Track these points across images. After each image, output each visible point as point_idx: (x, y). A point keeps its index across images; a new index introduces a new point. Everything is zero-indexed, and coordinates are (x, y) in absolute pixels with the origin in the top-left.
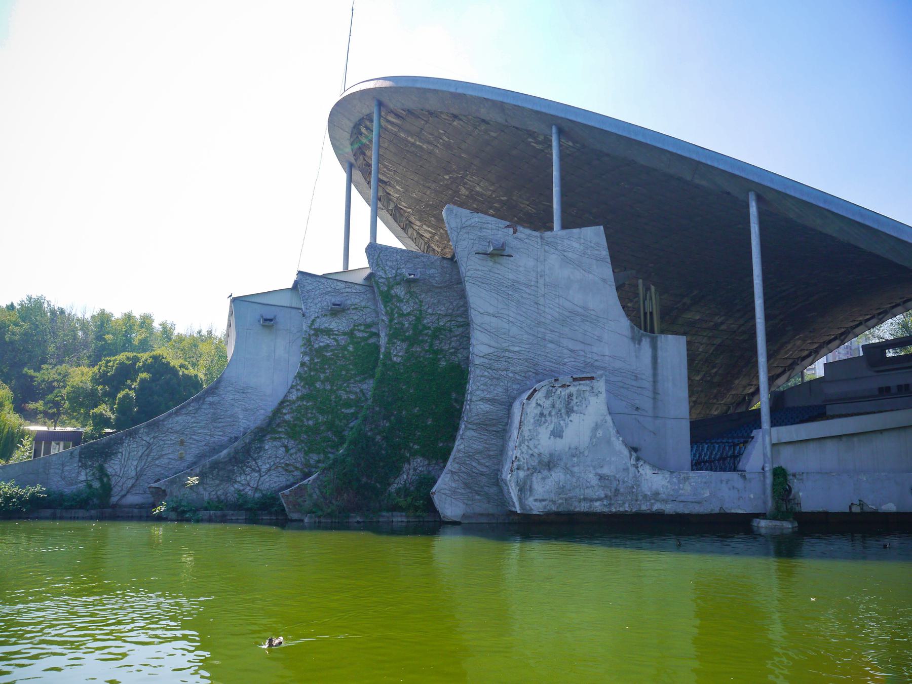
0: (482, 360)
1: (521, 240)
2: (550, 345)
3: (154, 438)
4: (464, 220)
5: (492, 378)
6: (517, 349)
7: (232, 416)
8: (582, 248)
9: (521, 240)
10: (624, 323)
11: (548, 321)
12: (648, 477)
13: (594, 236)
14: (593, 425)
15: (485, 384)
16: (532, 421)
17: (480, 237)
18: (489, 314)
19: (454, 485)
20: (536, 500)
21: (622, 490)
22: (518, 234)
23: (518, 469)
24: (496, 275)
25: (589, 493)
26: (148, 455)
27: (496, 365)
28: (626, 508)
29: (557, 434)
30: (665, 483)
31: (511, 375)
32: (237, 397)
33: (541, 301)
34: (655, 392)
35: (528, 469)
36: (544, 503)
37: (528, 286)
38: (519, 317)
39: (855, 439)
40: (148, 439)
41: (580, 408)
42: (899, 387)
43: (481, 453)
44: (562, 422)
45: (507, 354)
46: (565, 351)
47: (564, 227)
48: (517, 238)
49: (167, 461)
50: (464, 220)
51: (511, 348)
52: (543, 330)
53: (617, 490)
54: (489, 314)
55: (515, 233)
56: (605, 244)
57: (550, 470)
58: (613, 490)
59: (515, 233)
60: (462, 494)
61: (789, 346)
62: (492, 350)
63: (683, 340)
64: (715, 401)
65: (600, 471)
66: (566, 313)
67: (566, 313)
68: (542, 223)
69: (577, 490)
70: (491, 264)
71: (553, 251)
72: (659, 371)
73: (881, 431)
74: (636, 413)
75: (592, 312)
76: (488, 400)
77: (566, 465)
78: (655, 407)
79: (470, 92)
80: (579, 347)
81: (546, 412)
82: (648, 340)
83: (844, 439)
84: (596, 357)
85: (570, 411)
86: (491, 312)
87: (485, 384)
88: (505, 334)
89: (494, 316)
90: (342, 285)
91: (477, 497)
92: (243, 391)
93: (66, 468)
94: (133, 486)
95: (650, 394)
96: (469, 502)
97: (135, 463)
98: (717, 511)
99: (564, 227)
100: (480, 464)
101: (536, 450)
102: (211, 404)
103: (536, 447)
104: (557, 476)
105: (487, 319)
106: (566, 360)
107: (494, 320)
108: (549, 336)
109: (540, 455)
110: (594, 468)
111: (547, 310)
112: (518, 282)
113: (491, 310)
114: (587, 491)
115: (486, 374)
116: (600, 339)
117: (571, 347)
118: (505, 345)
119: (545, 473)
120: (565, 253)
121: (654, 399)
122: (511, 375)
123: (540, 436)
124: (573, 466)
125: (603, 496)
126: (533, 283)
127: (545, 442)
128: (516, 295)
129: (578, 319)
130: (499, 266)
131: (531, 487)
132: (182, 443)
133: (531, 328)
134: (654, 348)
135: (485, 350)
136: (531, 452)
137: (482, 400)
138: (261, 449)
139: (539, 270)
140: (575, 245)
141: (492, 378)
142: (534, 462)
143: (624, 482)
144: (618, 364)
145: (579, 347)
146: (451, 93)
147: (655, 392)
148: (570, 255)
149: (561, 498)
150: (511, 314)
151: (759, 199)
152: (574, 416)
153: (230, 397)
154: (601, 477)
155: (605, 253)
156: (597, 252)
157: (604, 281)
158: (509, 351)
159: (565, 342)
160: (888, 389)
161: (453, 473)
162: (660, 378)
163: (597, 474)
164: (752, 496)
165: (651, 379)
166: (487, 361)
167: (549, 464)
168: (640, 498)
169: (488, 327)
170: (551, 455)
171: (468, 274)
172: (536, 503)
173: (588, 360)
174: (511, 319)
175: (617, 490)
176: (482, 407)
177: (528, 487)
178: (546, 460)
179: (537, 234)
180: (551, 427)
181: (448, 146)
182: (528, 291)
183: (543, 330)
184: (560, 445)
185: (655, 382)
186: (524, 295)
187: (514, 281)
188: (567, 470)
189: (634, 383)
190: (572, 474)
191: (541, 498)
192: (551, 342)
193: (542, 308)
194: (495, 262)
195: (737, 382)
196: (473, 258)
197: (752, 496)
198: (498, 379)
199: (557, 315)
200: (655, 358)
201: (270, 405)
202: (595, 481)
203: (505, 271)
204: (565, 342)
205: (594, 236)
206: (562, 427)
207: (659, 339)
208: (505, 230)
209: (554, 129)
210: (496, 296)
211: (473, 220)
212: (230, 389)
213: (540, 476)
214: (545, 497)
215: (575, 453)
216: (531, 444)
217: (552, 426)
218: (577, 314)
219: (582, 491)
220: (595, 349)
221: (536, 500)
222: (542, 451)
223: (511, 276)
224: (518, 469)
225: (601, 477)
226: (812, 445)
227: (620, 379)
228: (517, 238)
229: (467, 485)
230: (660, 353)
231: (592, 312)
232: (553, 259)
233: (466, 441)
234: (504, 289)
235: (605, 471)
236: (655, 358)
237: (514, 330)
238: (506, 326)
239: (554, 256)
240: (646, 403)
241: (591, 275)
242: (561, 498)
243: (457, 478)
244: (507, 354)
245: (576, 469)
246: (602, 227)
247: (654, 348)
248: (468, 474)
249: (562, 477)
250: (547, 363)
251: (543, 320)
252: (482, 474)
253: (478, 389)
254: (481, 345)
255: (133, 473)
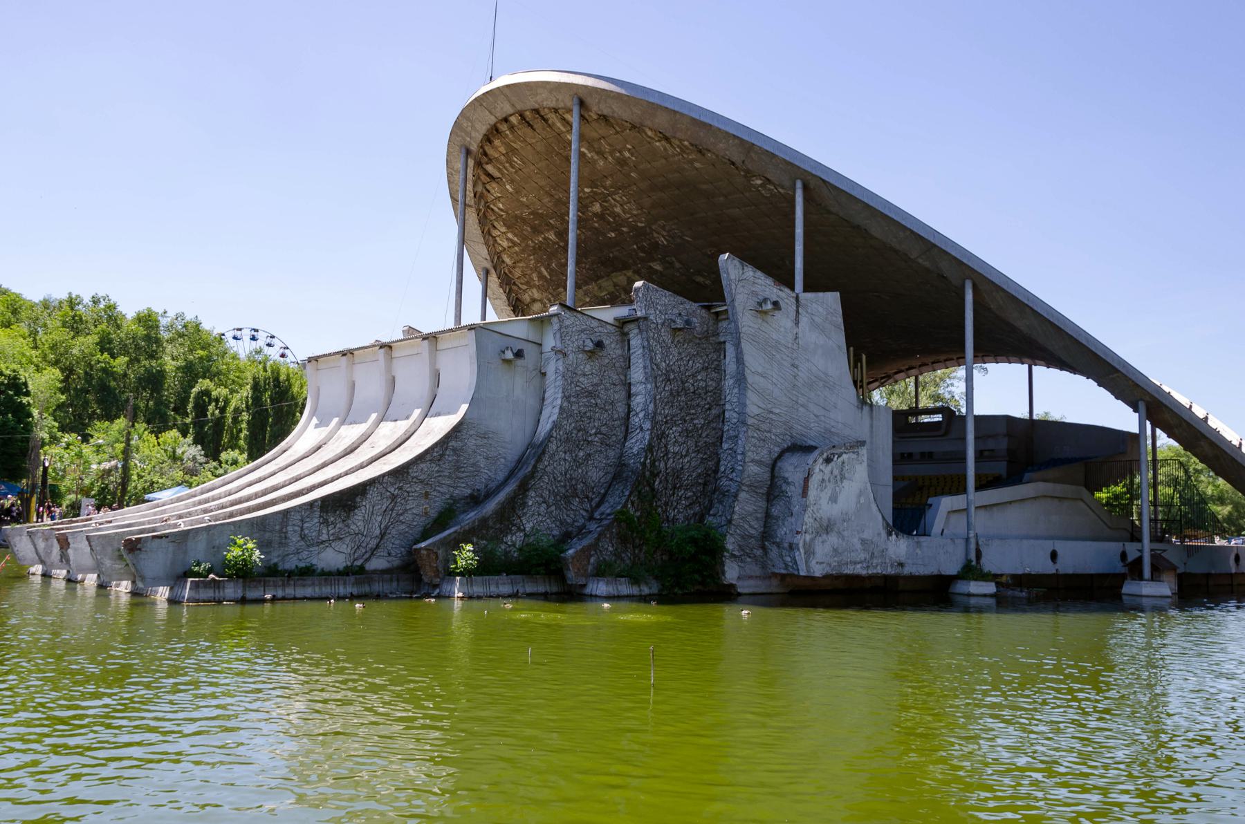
3: (400, 488)
5: (759, 440)
7: (473, 465)
13: (832, 300)
26: (392, 510)
28: (879, 570)
29: (834, 499)
32: (479, 442)
39: (995, 509)
40: (392, 490)
42: (923, 455)
45: (771, 416)
49: (410, 517)
54: (759, 374)
73: (1010, 503)
79: (715, 123)
80: (821, 412)
81: (826, 478)
85: (843, 478)
90: (595, 324)
92: (484, 436)
93: (306, 525)
94: (378, 546)
97: (379, 519)
98: (936, 572)
99: (807, 289)
100: (751, 526)
102: (454, 450)
105: (757, 378)
107: (762, 380)
119: (824, 536)
132: (427, 494)
135: (756, 411)
137: (752, 461)
138: (524, 504)
140: (821, 309)
141: (759, 440)
145: (822, 412)
146: (693, 119)
152: (846, 483)
153: (472, 443)
154: (863, 541)
155: (840, 320)
160: (910, 455)
167: (827, 528)
170: (829, 520)
181: (622, 162)
200: (872, 426)
201: (512, 453)
202: (859, 546)
205: (832, 300)
209: (799, 184)
212: (472, 432)
215: (846, 519)
225: (863, 541)
235: (865, 536)
238: (770, 387)
244: (771, 416)
245: (845, 533)
248: (743, 537)
252: (751, 536)
255: (377, 532)
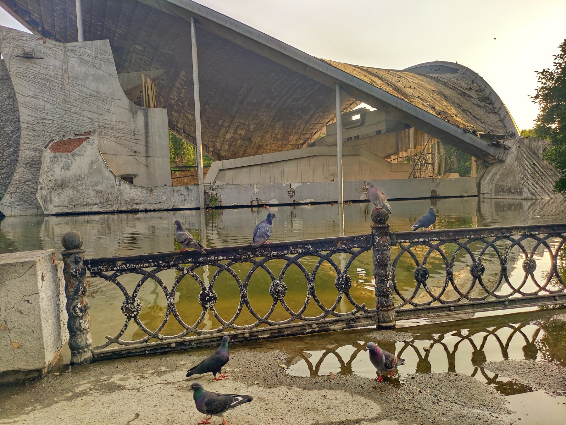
0: (27, 125)
1: (49, 48)
2: (74, 115)
4: (5, 34)
5: (34, 136)
6: (51, 118)
8: (94, 54)
9: (49, 48)
10: (125, 101)
11: (72, 100)
12: (127, 191)
14: (90, 162)
15: (30, 140)
16: (49, 160)
17: (18, 46)
18: (29, 96)
19: (12, 200)
20: (55, 206)
21: (110, 199)
22: (46, 44)
23: (41, 189)
24: (33, 71)
25: (89, 201)
27: (37, 128)
30: (138, 193)
31: (48, 134)
33: (67, 87)
34: (147, 142)
35: (48, 189)
36: (60, 208)
37: (56, 78)
38: (51, 98)
39: (271, 166)
41: (80, 152)
43: (30, 180)
44: (69, 161)
45: (44, 121)
46: (85, 119)
47: (86, 39)
48: (46, 47)
50: (5, 34)
51: (47, 117)
52: (69, 106)
53: (107, 199)
54: (29, 96)
55: (44, 43)
56: (111, 51)
57: (63, 189)
58: (105, 198)
59: (44, 43)
60: (19, 205)
61: (316, 116)
62: (33, 119)
63: (165, 110)
64: (281, 148)
65: (95, 188)
66: (84, 95)
67: (84, 95)
68: (66, 36)
69: (82, 200)
70: (28, 64)
71: (73, 55)
72: (150, 130)
74: (135, 154)
75: (103, 95)
76: (33, 149)
77: (73, 185)
78: (147, 151)
82: (142, 111)
83: (264, 166)
84: (106, 122)
86: (31, 95)
87: (30, 140)
88: (42, 108)
89: (33, 97)
91: (29, 206)
95: (143, 143)
96: (24, 210)
99: (86, 39)
100: (30, 187)
101: (53, 178)
103: (52, 176)
104: (68, 192)
106: (86, 124)
107: (33, 99)
108: (73, 110)
109: (55, 180)
110: (92, 186)
111: (71, 93)
112: (49, 76)
113: (31, 94)
114: (88, 200)
115: (30, 133)
116: (109, 111)
117: (88, 116)
118: (42, 115)
119: (60, 191)
120: (82, 57)
121: (146, 146)
122: (48, 134)
123: (55, 169)
124: (78, 186)
125: (99, 202)
126: (60, 77)
127: (58, 173)
128: (48, 84)
129: (93, 99)
130: (34, 65)
131: (50, 199)
133: (60, 105)
134: (146, 116)
136: (49, 179)
139: (64, 68)
140: (88, 51)
141: (34, 136)
142: (52, 184)
143: (111, 194)
144: (121, 126)
147: (147, 142)
148: (86, 58)
149: (71, 205)
150: (45, 96)
151: (196, 21)
152: (77, 157)
154: (97, 192)
155: (111, 57)
156: (105, 57)
157: (110, 74)
158: (45, 119)
159: (85, 113)
161: (11, 193)
162: (150, 134)
163: (94, 190)
164: (192, 199)
165: (144, 135)
166: (30, 126)
167: (62, 185)
168: (123, 202)
169: (29, 105)
170: (63, 180)
171: (11, 70)
172: (55, 208)
173: (102, 124)
174: (45, 99)
175: (107, 199)
176: (29, 153)
177: (49, 199)
178: (60, 183)
179: (61, 44)
180: (62, 164)
182: (56, 81)
183: (69, 106)
184: (68, 174)
185: (147, 136)
186: (54, 84)
187: (46, 75)
188: (73, 188)
189: (133, 137)
190: (78, 191)
191: (58, 205)
192: (75, 113)
193: (66, 92)
194: (31, 63)
195: (291, 137)
196: (14, 60)
197: (192, 199)
198: (39, 136)
199: (78, 97)
200: (146, 124)
202: (93, 194)
203: (35, 68)
204: (85, 113)
206: (69, 164)
207: (149, 111)
208: (37, 42)
210: (34, 85)
211: (11, 34)
213: (56, 192)
214: (60, 204)
215: (79, 178)
216: (49, 174)
217: (63, 163)
218: (93, 96)
219: (85, 200)
220: (106, 117)
221: (55, 206)
222: (57, 178)
223: (43, 72)
224: (41, 189)
225: (97, 192)
226: (245, 170)
227: (123, 135)
228: (46, 47)
229: (21, 200)
230: (150, 119)
231: (103, 95)
232: (73, 61)
233: (20, 173)
234: (39, 80)
235: (99, 188)
236: (146, 124)
237: (48, 106)
238: (43, 104)
239: (75, 59)
240: (142, 149)
241: (101, 72)
242: (71, 205)
243: (14, 196)
245: (80, 188)
246: (108, 40)
247: (146, 116)
249: (71, 192)
250: (74, 126)
251: (68, 99)
253: (25, 143)
254: (26, 115)
